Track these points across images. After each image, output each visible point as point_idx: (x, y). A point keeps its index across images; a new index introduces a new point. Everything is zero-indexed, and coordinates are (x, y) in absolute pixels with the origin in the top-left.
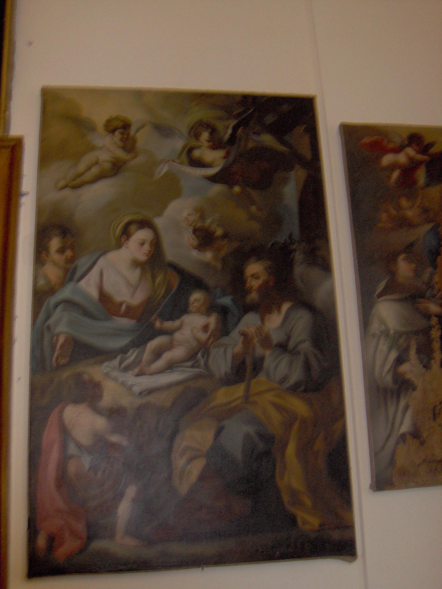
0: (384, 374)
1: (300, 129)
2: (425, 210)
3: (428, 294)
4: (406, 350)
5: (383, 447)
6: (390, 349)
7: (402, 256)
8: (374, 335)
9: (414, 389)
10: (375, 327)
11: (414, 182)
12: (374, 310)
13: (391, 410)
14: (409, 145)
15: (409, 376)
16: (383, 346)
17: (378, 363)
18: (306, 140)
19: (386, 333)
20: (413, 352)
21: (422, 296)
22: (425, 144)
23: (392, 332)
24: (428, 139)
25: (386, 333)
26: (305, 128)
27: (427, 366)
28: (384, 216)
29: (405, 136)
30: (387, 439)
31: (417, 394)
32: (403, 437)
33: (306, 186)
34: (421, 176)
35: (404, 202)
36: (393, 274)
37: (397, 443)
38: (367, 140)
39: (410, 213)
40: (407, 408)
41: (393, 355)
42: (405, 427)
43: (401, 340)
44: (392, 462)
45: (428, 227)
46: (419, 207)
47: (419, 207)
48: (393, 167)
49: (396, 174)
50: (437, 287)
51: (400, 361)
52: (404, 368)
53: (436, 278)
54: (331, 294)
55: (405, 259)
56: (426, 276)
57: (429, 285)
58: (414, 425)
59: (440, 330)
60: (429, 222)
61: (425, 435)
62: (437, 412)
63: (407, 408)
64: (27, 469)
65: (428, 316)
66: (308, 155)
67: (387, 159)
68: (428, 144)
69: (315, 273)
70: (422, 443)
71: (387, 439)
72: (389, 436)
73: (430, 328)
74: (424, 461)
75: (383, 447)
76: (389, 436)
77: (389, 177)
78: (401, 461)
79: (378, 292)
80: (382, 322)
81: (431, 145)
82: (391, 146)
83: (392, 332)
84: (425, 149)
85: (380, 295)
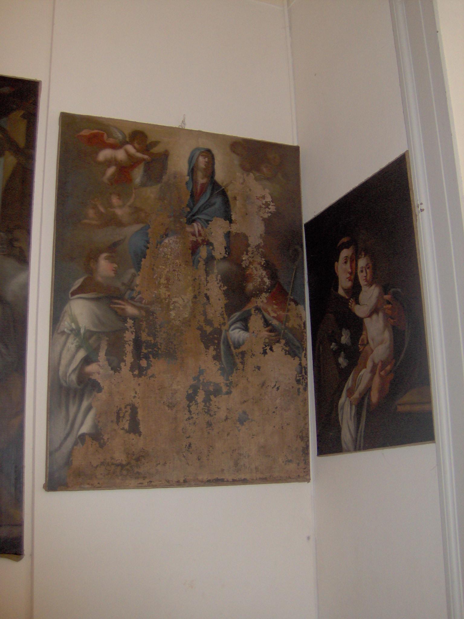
0: (68, 374)
1: (17, 115)
2: (136, 210)
3: (127, 296)
4: (97, 350)
5: (61, 445)
6: (78, 348)
7: (104, 255)
8: (63, 333)
9: (100, 390)
10: (66, 324)
11: (130, 180)
12: (67, 308)
13: (73, 410)
14: (131, 142)
15: (95, 377)
16: (72, 344)
17: (64, 362)
18: (22, 126)
19: (76, 332)
20: (102, 354)
21: (121, 297)
22: (148, 142)
23: (82, 331)
24: (152, 138)
25: (76, 332)
26: (24, 114)
27: (116, 369)
28: (91, 212)
29: (127, 132)
30: (66, 438)
31: (103, 396)
32: (82, 438)
33: (14, 174)
34: (138, 175)
35: (115, 200)
36: (91, 272)
37: (76, 444)
38: (85, 132)
39: (119, 212)
40: (89, 408)
41: (81, 354)
42: (86, 428)
43: (91, 341)
44: (68, 462)
45: (136, 227)
46: (130, 206)
47: (130, 206)
48: (109, 163)
49: (111, 171)
50: (137, 289)
51: (87, 361)
52: (91, 368)
53: (138, 281)
54: (25, 287)
55: (106, 258)
56: (127, 278)
57: (130, 286)
58: (95, 426)
59: (134, 333)
60: (138, 223)
61: (106, 437)
62: (121, 415)
63: (89, 408)
64: (27, 367)
65: (123, 317)
66: (21, 141)
67: (105, 154)
68: (152, 142)
69: (10, 264)
70: (102, 446)
71: (66, 438)
72: (68, 435)
73: (125, 329)
74: (102, 463)
75: (61, 445)
76: (68, 435)
77: (104, 174)
78: (78, 461)
79: (75, 287)
80: (74, 320)
81: (155, 144)
82: (111, 141)
83: (82, 331)
84: (146, 147)
85: (73, 294)
